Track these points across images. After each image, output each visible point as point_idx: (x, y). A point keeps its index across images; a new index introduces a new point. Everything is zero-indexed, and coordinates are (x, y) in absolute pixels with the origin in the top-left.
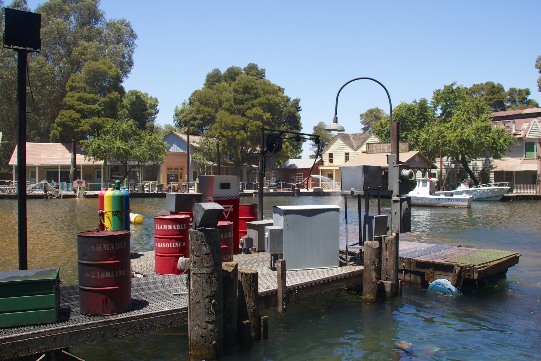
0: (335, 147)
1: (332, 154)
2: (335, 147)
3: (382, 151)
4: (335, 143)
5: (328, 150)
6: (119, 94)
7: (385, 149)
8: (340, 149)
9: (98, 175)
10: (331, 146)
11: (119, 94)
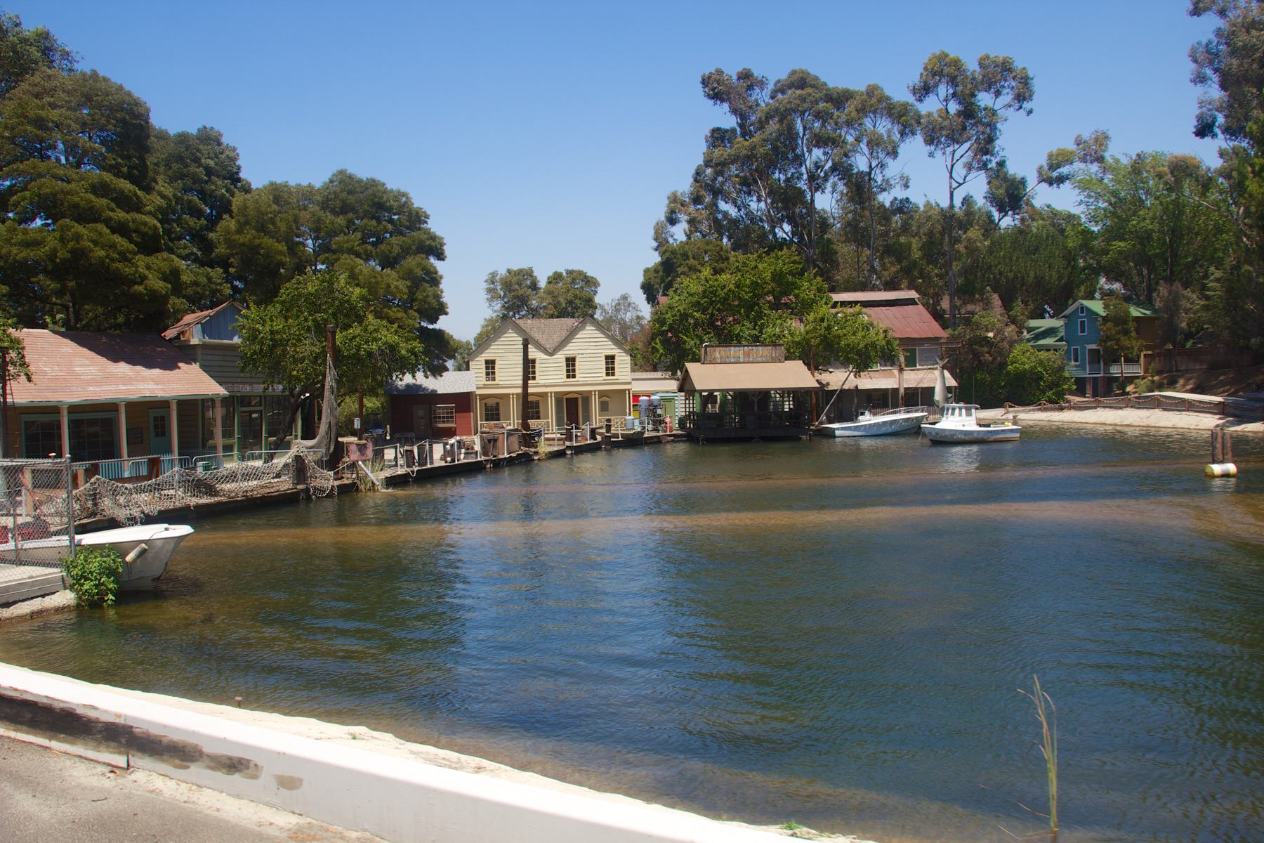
0: (500, 347)
1: (493, 362)
2: (500, 347)
3: (733, 360)
4: (500, 337)
5: (482, 353)
6: (199, 219)
7: (739, 358)
8: (514, 351)
9: (156, 427)
10: (490, 346)
11: (199, 219)
